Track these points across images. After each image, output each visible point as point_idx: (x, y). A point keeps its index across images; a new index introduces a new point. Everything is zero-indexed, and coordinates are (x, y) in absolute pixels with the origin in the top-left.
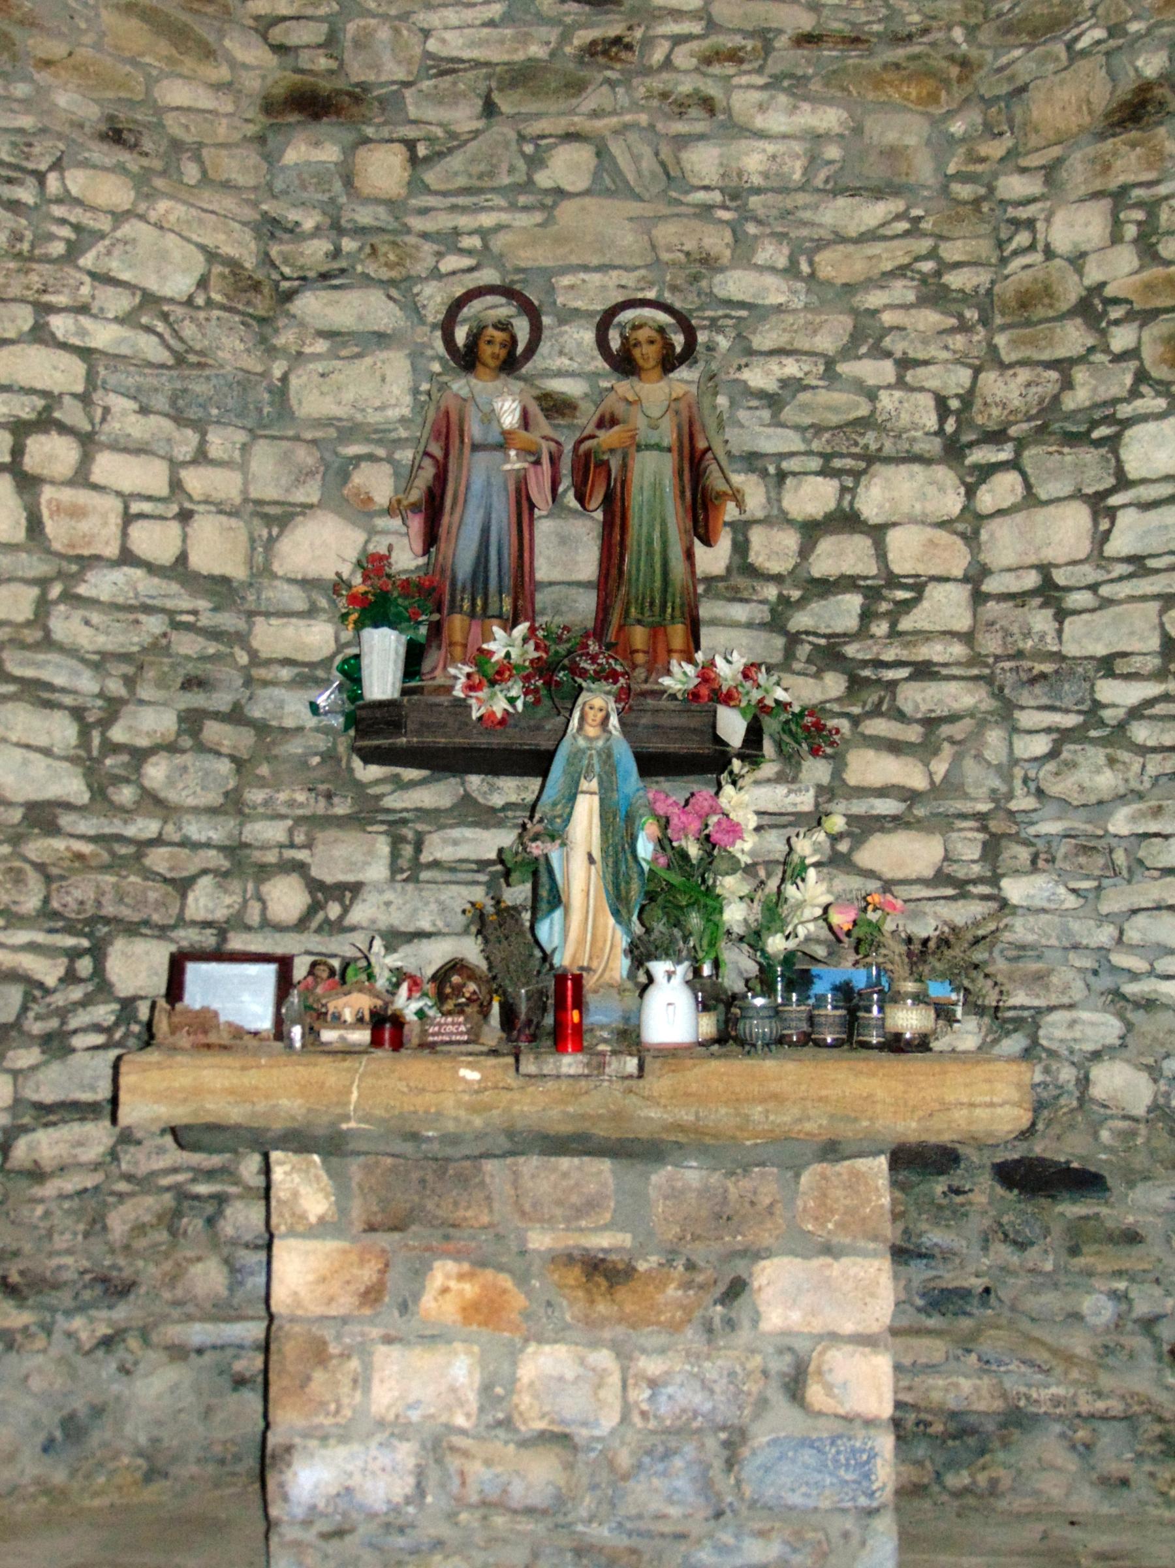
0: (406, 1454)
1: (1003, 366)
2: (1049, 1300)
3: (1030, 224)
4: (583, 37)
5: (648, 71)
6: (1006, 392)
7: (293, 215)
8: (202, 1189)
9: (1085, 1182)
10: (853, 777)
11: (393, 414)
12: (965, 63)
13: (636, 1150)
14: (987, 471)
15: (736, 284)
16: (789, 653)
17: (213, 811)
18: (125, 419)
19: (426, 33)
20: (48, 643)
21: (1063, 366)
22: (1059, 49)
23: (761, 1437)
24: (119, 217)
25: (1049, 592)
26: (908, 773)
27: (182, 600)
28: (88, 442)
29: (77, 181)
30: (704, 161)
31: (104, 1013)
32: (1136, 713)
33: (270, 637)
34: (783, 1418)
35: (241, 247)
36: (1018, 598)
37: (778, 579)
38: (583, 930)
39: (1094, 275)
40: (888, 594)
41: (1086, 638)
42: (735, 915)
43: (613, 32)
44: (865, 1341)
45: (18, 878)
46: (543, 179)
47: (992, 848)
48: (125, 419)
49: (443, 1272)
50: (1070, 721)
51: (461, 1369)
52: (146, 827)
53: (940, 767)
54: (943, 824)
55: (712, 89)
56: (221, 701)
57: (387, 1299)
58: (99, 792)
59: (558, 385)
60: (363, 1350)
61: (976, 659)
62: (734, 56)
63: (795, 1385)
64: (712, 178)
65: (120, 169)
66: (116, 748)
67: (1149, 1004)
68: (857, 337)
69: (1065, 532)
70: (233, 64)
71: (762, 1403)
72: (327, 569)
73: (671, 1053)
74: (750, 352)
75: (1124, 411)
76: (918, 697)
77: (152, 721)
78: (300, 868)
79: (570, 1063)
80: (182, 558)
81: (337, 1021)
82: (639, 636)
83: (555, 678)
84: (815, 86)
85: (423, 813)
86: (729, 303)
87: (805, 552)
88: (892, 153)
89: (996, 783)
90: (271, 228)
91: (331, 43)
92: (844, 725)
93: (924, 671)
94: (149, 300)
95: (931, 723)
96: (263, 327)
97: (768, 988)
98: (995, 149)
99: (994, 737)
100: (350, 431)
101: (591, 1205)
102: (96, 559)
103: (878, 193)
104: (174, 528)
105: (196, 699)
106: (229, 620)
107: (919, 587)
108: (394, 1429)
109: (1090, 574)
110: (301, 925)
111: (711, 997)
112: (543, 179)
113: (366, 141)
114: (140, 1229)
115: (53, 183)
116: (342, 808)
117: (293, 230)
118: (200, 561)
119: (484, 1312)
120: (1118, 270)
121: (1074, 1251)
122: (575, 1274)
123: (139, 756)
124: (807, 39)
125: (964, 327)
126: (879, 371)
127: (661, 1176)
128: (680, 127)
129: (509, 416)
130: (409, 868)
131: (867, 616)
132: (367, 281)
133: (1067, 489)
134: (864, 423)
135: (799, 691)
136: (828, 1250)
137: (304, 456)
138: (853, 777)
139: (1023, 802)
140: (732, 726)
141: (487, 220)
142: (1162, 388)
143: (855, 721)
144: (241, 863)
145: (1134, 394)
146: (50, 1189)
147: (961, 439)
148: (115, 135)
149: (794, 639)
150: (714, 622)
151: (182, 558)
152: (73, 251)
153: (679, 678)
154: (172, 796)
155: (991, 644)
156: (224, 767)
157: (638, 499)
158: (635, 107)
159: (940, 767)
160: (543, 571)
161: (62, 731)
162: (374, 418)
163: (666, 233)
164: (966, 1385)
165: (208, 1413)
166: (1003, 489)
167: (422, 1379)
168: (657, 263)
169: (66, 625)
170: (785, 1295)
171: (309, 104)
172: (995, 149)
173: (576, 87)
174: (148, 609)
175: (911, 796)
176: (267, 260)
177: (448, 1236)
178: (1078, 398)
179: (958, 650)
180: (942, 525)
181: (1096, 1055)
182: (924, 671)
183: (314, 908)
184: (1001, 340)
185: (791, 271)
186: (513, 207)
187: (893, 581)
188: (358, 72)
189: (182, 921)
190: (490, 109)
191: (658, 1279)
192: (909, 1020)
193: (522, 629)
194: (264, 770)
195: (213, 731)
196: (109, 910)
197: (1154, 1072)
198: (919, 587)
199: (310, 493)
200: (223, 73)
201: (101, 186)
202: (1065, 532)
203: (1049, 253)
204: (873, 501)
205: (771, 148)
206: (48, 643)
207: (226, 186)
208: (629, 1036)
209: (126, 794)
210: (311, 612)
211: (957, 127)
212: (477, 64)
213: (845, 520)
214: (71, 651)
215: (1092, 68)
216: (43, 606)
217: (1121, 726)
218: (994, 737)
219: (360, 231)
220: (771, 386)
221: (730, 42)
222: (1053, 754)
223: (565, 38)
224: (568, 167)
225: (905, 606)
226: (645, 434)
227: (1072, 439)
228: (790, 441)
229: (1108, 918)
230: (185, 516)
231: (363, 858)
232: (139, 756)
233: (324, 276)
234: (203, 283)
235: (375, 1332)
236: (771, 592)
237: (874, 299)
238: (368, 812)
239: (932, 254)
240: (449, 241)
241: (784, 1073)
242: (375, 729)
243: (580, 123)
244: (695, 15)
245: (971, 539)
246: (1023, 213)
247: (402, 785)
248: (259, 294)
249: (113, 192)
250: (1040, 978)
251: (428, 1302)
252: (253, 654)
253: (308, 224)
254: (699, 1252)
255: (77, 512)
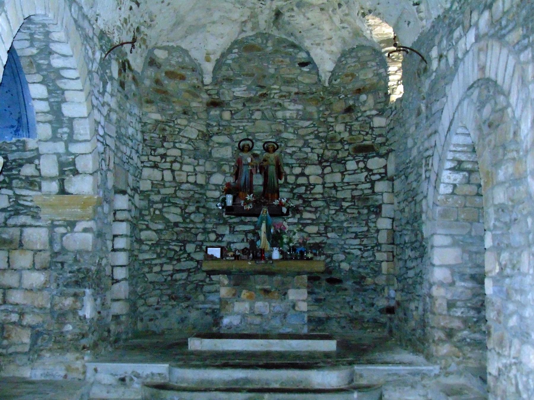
0: (239, 317)
1: (328, 150)
2: (333, 300)
3: (332, 126)
4: (261, 93)
5: (271, 99)
6: (329, 154)
7: (212, 123)
8: (201, 283)
9: (339, 281)
10: (304, 217)
11: (229, 157)
12: (323, 98)
13: (272, 274)
14: (325, 167)
15: (285, 135)
16: (293, 197)
17: (201, 222)
18: (187, 159)
19: (234, 92)
20: (176, 197)
21: (337, 151)
22: (337, 98)
23: (289, 314)
24: (186, 126)
25: (335, 187)
26: (313, 216)
27: (196, 189)
28: (181, 164)
29: (179, 121)
30: (280, 114)
31: (186, 255)
32: (347, 207)
33: (210, 194)
34: (292, 312)
35: (204, 129)
36: (330, 188)
37: (292, 184)
38: (263, 243)
39: (342, 136)
40: (309, 187)
41: (340, 195)
42: (285, 240)
43: (264, 92)
44: (304, 301)
45: (173, 234)
46: (253, 117)
47: (326, 228)
48: (187, 159)
49: (244, 292)
50: (338, 208)
51: (247, 305)
52: (191, 226)
53: (318, 215)
54: (318, 224)
55: (281, 102)
56: (202, 205)
57: (237, 296)
58: (184, 220)
59: (256, 152)
60: (233, 303)
61: (324, 197)
62: (285, 96)
63: (294, 307)
64: (281, 117)
65: (185, 118)
66: (187, 213)
67: (349, 253)
68: (305, 144)
69: (337, 177)
70: (202, 98)
71: (289, 310)
72: (220, 183)
73: (276, 260)
74: (287, 146)
75: (346, 159)
76: (314, 204)
77: (192, 209)
78: (215, 232)
79: (263, 262)
80: (196, 182)
81: (228, 256)
82: (270, 195)
83: (258, 203)
84: (298, 101)
85: (234, 223)
86: (284, 138)
87: (296, 179)
88: (311, 113)
89: (326, 218)
90: (208, 125)
91: (218, 94)
92: (302, 208)
93: (316, 199)
94: (190, 139)
95: (316, 208)
96: (207, 142)
97: (289, 251)
98: (327, 113)
99: (326, 210)
100: (222, 159)
101: (265, 282)
102: (183, 183)
103: (309, 120)
104: (194, 177)
105: (198, 205)
106: (202, 191)
107: (314, 185)
108: (238, 314)
109: (341, 185)
110: (215, 241)
111: (282, 252)
112: (253, 117)
113: (224, 110)
114: (191, 290)
115: (176, 122)
116: (221, 222)
117: (212, 126)
118: (198, 182)
119: (250, 297)
120: (346, 135)
121: (338, 292)
122: (262, 292)
123: (190, 214)
124: (297, 93)
125: (322, 142)
126: (308, 150)
127: (275, 278)
128: (276, 108)
129: (249, 160)
130: (233, 232)
131: (306, 190)
132: (224, 134)
133: (338, 171)
134: (306, 158)
135: (295, 203)
136: (298, 288)
137: (215, 164)
138: (304, 217)
139: (330, 221)
140: (284, 210)
141: (244, 124)
142: (352, 156)
143: (304, 207)
144: (205, 231)
145: (348, 156)
146: (178, 283)
147: (321, 161)
148: (185, 113)
149: (294, 194)
150: (282, 191)
151: (196, 182)
152: (179, 132)
153: (276, 202)
154: (195, 220)
155: (326, 195)
156: (202, 215)
157: (270, 173)
158: (268, 105)
159: (318, 215)
160: (254, 183)
161: (179, 211)
162: (225, 157)
163: (273, 126)
164: (321, 313)
165: (202, 318)
166: (328, 170)
167: (241, 307)
168: (272, 131)
169: (179, 194)
170: (292, 295)
171: (214, 104)
172: (327, 113)
173: (258, 101)
174: (191, 190)
175: (313, 220)
176: (208, 131)
177: (245, 287)
178: (340, 156)
179: (321, 196)
180: (318, 175)
181: (341, 261)
182: (316, 199)
183: (217, 238)
184: (328, 145)
185: (294, 133)
186: (248, 122)
187: (310, 184)
188: (222, 98)
189: (196, 241)
190: (244, 105)
191: (274, 292)
192: (310, 255)
193: (252, 195)
194: (208, 216)
195: (201, 210)
196: (186, 239)
197: (350, 264)
198: (314, 185)
199: (215, 170)
200: (200, 100)
201: (182, 121)
202: (337, 177)
203: (335, 132)
204: (307, 171)
205: (291, 112)
206: (176, 197)
207: (201, 119)
208: (270, 258)
209: (188, 220)
210: (216, 190)
211: (321, 109)
212: (242, 98)
213: (302, 174)
214: (179, 198)
215: (342, 102)
216: (175, 191)
217: (345, 209)
218: (326, 210)
219: (223, 126)
220: (291, 152)
221: (284, 94)
222: (335, 213)
223: (257, 93)
224: (257, 115)
225: (312, 189)
226: (271, 163)
227: (339, 163)
228: (294, 161)
229: (343, 240)
230: (196, 175)
231: (225, 230)
232: (190, 214)
233: (217, 133)
234: (198, 136)
235: (235, 300)
236: (291, 186)
237: (307, 138)
238: (225, 223)
239: (317, 130)
240: (238, 128)
241: (292, 263)
242: (229, 210)
243: (259, 107)
244: (278, 89)
245: (323, 178)
246: (332, 124)
247: (231, 218)
248: (206, 137)
249: (184, 122)
250: (333, 249)
251: (242, 296)
252: (207, 198)
253: (214, 124)
254: (280, 288)
255: (180, 175)
